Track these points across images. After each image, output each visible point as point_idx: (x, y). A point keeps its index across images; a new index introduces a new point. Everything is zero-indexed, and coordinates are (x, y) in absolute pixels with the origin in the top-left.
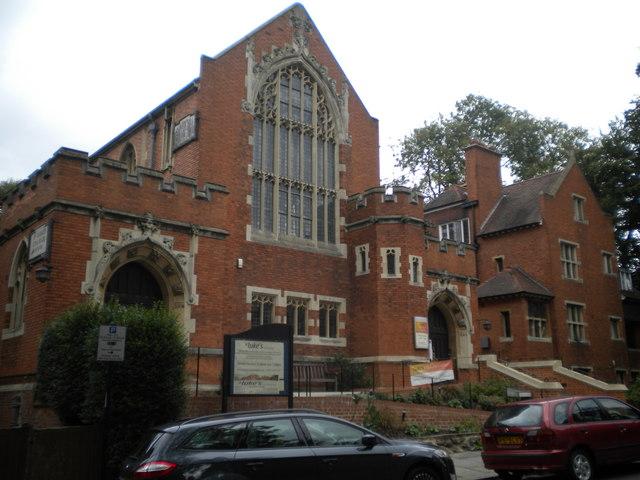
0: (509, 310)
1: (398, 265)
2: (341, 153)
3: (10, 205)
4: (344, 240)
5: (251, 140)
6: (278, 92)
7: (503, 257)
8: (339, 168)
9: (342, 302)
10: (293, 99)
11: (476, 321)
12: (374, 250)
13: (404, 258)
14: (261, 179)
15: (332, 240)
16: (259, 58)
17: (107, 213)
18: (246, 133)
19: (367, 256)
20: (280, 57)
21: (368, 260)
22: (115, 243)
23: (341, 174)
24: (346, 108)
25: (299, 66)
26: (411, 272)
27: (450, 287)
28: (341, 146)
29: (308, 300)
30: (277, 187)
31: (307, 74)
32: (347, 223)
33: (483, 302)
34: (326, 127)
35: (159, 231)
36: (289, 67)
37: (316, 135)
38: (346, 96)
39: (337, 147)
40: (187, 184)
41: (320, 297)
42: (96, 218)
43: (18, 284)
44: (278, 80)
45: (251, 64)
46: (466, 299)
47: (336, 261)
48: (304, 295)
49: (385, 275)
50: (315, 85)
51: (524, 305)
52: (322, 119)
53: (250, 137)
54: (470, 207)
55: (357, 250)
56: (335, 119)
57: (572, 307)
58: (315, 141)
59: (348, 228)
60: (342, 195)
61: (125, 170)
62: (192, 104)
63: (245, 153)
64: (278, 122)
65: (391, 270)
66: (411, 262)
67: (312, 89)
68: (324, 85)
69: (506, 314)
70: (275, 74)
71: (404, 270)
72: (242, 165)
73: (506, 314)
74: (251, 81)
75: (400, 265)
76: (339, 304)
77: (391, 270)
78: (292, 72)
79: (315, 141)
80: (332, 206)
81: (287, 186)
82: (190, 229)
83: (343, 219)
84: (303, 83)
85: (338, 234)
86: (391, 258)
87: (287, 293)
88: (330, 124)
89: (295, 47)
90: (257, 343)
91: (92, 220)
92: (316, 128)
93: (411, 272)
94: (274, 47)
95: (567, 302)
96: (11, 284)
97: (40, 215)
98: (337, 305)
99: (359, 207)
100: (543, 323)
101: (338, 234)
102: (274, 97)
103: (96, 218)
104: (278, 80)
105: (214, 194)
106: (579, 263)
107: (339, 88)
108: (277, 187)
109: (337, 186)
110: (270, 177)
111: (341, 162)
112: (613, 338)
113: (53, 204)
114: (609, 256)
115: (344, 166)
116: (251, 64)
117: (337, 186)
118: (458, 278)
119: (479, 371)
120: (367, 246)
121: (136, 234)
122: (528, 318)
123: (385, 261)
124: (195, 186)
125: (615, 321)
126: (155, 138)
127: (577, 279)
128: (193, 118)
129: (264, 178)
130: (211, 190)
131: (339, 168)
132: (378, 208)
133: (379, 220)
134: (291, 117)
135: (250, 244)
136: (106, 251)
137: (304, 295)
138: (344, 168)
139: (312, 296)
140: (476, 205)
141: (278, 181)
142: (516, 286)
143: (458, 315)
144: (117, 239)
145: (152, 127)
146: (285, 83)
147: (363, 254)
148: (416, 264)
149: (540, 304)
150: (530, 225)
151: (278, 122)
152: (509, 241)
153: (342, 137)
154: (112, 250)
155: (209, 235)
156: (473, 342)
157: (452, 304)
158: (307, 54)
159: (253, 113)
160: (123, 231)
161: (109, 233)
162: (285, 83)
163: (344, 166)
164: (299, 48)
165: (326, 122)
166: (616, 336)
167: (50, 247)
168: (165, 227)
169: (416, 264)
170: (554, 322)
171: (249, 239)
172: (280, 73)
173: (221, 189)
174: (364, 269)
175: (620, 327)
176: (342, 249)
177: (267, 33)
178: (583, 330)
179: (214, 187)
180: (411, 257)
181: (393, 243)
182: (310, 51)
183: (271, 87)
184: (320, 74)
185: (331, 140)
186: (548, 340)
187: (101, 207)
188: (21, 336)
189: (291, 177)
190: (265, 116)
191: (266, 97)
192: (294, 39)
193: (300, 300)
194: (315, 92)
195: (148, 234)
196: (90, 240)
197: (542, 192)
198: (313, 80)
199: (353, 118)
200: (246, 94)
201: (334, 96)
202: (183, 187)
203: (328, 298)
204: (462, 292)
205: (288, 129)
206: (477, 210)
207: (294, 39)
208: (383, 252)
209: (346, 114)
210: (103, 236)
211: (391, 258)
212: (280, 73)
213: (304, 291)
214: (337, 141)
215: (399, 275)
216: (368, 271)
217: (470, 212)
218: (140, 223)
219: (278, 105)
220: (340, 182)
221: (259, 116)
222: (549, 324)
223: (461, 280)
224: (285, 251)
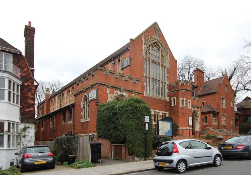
0: (207, 116)
1: (185, 103)
2: (167, 70)
3: (78, 85)
4: (168, 96)
5: (145, 66)
6: (151, 51)
7: (204, 102)
8: (167, 75)
9: (167, 113)
10: (154, 53)
11: (201, 119)
12: (178, 99)
13: (186, 101)
14: (147, 78)
15: (165, 96)
16: (146, 40)
17: (111, 87)
18: (143, 64)
19: (175, 100)
20: (151, 40)
21: (176, 101)
22: (113, 95)
23: (167, 77)
24: (169, 56)
25: (156, 43)
26: (188, 105)
27: (195, 109)
28: (167, 68)
29: (159, 112)
30: (151, 80)
31: (158, 46)
32: (169, 91)
33: (203, 113)
34: (163, 62)
35: (124, 92)
36: (153, 43)
37: (161, 64)
38: (169, 53)
39: (166, 69)
40: (130, 78)
41: (162, 112)
42: (108, 88)
43: (84, 107)
44: (151, 47)
45: (144, 42)
46: (199, 113)
47: (166, 102)
48: (158, 111)
49: (181, 106)
50: (160, 49)
51: (212, 114)
52: (162, 60)
53: (144, 65)
54: (195, 88)
55: (172, 99)
56: (165, 60)
57: (223, 115)
58: (160, 66)
59: (169, 92)
60: (167, 83)
61: (115, 74)
62: (128, 54)
63: (142, 70)
64: (151, 61)
65: (183, 104)
66: (188, 102)
67: (159, 51)
68: (163, 49)
69: (206, 117)
70: (150, 46)
71: (186, 104)
72: (142, 73)
73: (206, 117)
74: (144, 47)
75: (185, 103)
76: (167, 114)
77: (183, 104)
78: (154, 45)
79: (160, 66)
80: (164, 86)
81: (153, 80)
82: (132, 91)
83: (168, 90)
84: (157, 48)
85: (166, 95)
86: (183, 100)
87: (154, 110)
88: (164, 61)
89: (155, 37)
90: (164, 122)
91: (107, 88)
92: (161, 63)
93: (188, 105)
94: (150, 37)
95: (222, 114)
96: (82, 107)
97: (92, 87)
98: (166, 114)
99: (173, 86)
100: (216, 119)
101: (166, 95)
102: (149, 53)
103: (108, 88)
104: (151, 47)
105: (138, 81)
106: (226, 103)
107: (167, 50)
108: (151, 80)
109: (166, 80)
110: (149, 77)
111: (167, 73)
112: (232, 124)
113: (97, 83)
114: (232, 101)
115: (168, 74)
116: (144, 42)
117: (166, 80)
118: (197, 107)
119: (192, 130)
120: (175, 98)
121: (119, 93)
122: (212, 118)
123: (181, 101)
124: (133, 79)
125: (232, 119)
126: (114, 66)
127: (225, 108)
128: (129, 59)
129: (148, 77)
130: (137, 80)
131: (167, 75)
132: (179, 87)
133: (180, 90)
134: (154, 59)
135: (145, 97)
136: (111, 98)
137: (158, 111)
138: (168, 75)
139: (160, 111)
140: (197, 87)
141: (151, 79)
142: (208, 110)
143: (196, 117)
144: (114, 94)
145: (113, 62)
146: (152, 48)
147: (174, 100)
148: (189, 103)
149: (215, 114)
150: (213, 93)
151: (151, 61)
152: (207, 97)
153: (168, 66)
154: (113, 97)
155: (136, 93)
156: (200, 124)
157: (195, 114)
158: (158, 39)
159: (144, 58)
160: (115, 92)
161: (112, 93)
162: (152, 48)
163: (168, 74)
164: (156, 37)
165: (163, 61)
166: (233, 123)
167: (97, 96)
168: (127, 91)
169: (189, 103)
170: (218, 119)
171: (144, 95)
172: (151, 45)
173: (139, 80)
174: (174, 104)
175: (233, 121)
176: (168, 99)
177: (148, 32)
178: (225, 121)
179: (137, 79)
180: (188, 101)
181: (183, 96)
182: (159, 38)
183: (149, 50)
184: (162, 45)
185: (164, 66)
186: (217, 124)
187: (110, 84)
188: (89, 121)
189: (155, 77)
190: (147, 58)
191: (147, 53)
192: (155, 34)
193: (157, 112)
194: (160, 51)
195: (122, 92)
196: (107, 94)
197: (218, 83)
198: (160, 48)
199: (171, 60)
200: (143, 51)
201: (165, 53)
202: (129, 79)
203: (164, 112)
204: (198, 111)
205: (153, 63)
206: (197, 89)
207: (155, 34)
208: (181, 99)
209: (169, 58)
210: (110, 93)
211: (183, 100)
212: (151, 45)
213: (158, 110)
214: (166, 67)
215: (185, 106)
216: (175, 104)
217: (195, 89)
218: (119, 89)
219: (151, 55)
220: (167, 79)
221: (146, 59)
222: (217, 120)
223: (198, 107)
224: (154, 99)
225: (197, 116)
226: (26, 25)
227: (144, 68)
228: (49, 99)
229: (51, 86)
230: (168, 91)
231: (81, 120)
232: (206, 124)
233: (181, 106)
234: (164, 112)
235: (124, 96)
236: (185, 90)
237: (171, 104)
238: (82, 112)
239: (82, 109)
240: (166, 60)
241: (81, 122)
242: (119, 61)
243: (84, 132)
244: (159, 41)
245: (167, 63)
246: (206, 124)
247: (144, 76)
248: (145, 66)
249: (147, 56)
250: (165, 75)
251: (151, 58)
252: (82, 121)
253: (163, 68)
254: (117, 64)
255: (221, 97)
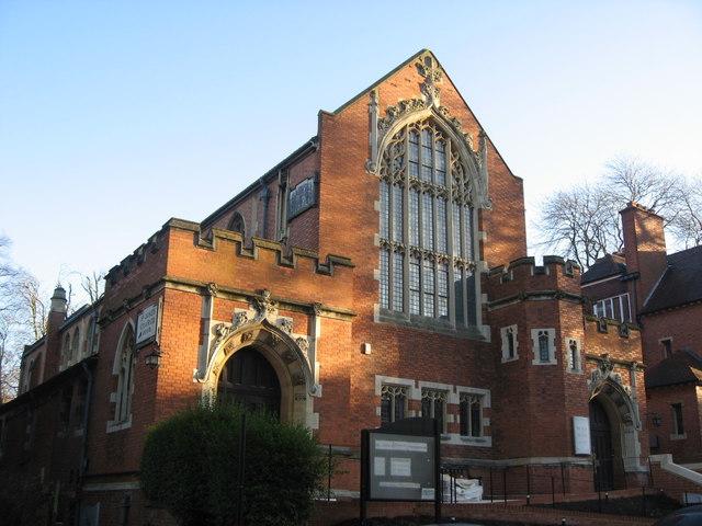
1: (552, 349)
4: (486, 321)
5: (378, 206)
7: (671, 338)
15: (473, 320)
19: (515, 339)
21: (516, 344)
29: (447, 391)
43: (123, 371)
47: (478, 344)
48: (442, 386)
49: (536, 362)
54: (630, 280)
55: (503, 332)
76: (482, 396)
85: (479, 314)
96: (116, 371)
101: (479, 314)
102: (402, 157)
120: (515, 327)
123: (536, 344)
137: (442, 386)
139: (451, 387)
174: (511, 354)
176: (485, 331)
193: (437, 391)
198: (445, 135)
203: (469, 390)
208: (535, 334)
215: (553, 361)
216: (516, 357)
217: (631, 286)
225: (624, 403)
226: (324, 109)
227: (377, 214)
228: (61, 332)
229: (91, 277)
230: (485, 300)
231: (109, 423)
232: (681, 437)
233: (536, 362)
234: (469, 390)
235: (272, 327)
236: (552, 294)
237: (501, 354)
238: (115, 390)
239: (116, 377)
240: (476, 181)
241: (109, 430)
242: (283, 188)
243: (681, 306)
244: (439, 114)
245: (477, 190)
246: (681, 437)
247: (377, 243)
248: (378, 206)
249: (393, 168)
250: (472, 235)
251: (410, 176)
252: (111, 428)
253: (466, 211)
254: (276, 201)
255: (660, 340)
